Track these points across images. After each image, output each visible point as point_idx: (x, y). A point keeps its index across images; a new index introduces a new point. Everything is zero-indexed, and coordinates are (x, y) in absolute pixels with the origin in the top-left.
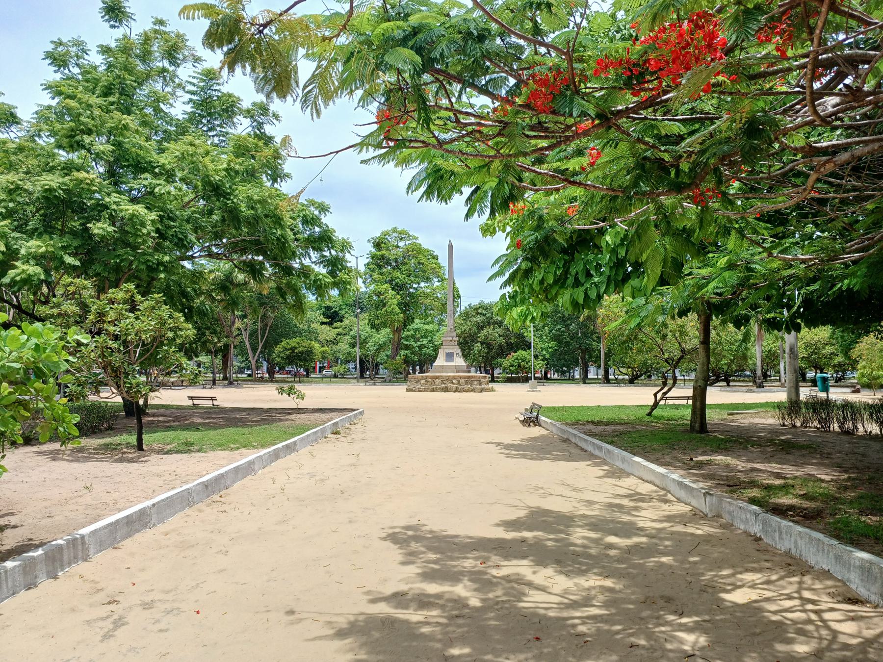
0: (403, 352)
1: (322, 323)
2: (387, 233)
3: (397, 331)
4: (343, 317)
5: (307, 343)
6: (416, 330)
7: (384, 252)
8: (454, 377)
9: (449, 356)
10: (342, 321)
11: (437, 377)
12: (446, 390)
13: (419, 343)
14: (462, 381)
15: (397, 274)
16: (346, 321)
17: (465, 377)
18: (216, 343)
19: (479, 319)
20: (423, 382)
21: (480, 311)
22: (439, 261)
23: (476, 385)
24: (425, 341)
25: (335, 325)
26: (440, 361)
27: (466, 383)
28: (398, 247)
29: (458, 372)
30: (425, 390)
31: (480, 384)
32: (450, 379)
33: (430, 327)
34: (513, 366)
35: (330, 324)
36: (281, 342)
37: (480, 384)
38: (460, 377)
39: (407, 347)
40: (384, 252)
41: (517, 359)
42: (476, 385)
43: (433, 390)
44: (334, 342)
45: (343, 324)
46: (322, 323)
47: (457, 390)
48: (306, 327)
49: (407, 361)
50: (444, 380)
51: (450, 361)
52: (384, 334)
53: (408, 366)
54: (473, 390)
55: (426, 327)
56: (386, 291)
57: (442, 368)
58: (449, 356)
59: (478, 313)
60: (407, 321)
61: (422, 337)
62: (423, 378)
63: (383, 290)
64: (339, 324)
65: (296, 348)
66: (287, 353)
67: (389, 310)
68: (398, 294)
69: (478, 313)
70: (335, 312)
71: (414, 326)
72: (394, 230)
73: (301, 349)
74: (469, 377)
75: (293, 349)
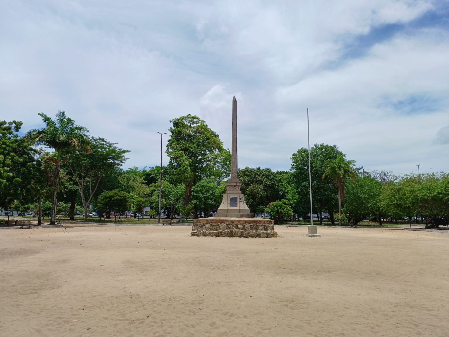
0: (194, 201)
1: (142, 183)
2: (183, 118)
3: (189, 186)
4: (157, 180)
5: (122, 193)
6: (202, 187)
7: (180, 128)
8: (239, 221)
9: (233, 201)
10: (155, 183)
11: (222, 222)
12: (231, 235)
13: (204, 195)
14: (247, 225)
15: (189, 144)
16: (159, 183)
17: (250, 222)
18: (39, 190)
19: (246, 178)
20: (208, 226)
21: (246, 173)
22: (219, 138)
23: (261, 230)
24: (208, 194)
25: (151, 185)
26: (224, 206)
27: (252, 228)
28: (190, 127)
29: (242, 216)
30: (210, 235)
31: (266, 229)
32: (235, 224)
33: (211, 185)
34: (272, 211)
35: (148, 184)
36: (103, 192)
37: (266, 229)
38: (246, 222)
39: (196, 198)
40: (180, 128)
41: (276, 206)
42: (261, 230)
43: (218, 235)
44: (151, 194)
45: (157, 184)
46: (142, 183)
47: (242, 236)
48: (125, 184)
49: (196, 208)
50: (229, 224)
51: (232, 207)
52: (181, 188)
53: (197, 211)
54: (259, 236)
55: (209, 185)
56: (181, 156)
57: (227, 213)
58: (233, 201)
59: (245, 175)
60: (196, 179)
61: (206, 191)
62: (208, 222)
63: (179, 155)
64: (154, 184)
65: (113, 197)
66: (106, 200)
67: (183, 169)
68: (190, 158)
69: (245, 175)
70: (153, 177)
71: (200, 183)
72: (189, 116)
73: (117, 198)
74: (254, 222)
75: (111, 197)
